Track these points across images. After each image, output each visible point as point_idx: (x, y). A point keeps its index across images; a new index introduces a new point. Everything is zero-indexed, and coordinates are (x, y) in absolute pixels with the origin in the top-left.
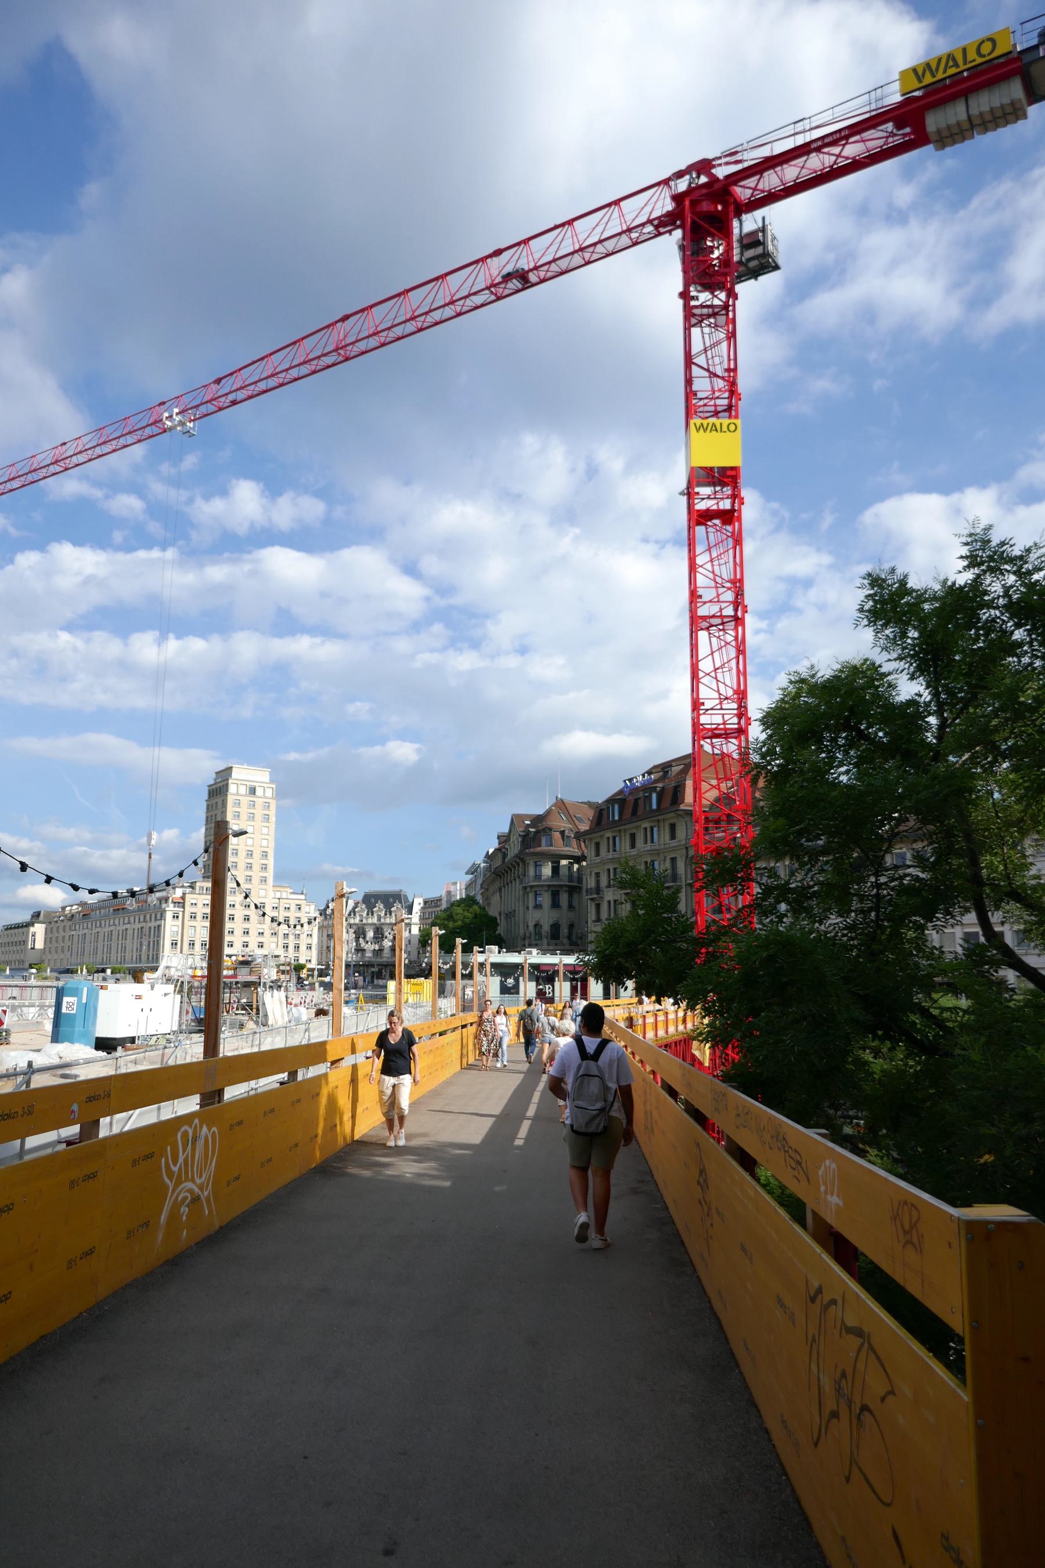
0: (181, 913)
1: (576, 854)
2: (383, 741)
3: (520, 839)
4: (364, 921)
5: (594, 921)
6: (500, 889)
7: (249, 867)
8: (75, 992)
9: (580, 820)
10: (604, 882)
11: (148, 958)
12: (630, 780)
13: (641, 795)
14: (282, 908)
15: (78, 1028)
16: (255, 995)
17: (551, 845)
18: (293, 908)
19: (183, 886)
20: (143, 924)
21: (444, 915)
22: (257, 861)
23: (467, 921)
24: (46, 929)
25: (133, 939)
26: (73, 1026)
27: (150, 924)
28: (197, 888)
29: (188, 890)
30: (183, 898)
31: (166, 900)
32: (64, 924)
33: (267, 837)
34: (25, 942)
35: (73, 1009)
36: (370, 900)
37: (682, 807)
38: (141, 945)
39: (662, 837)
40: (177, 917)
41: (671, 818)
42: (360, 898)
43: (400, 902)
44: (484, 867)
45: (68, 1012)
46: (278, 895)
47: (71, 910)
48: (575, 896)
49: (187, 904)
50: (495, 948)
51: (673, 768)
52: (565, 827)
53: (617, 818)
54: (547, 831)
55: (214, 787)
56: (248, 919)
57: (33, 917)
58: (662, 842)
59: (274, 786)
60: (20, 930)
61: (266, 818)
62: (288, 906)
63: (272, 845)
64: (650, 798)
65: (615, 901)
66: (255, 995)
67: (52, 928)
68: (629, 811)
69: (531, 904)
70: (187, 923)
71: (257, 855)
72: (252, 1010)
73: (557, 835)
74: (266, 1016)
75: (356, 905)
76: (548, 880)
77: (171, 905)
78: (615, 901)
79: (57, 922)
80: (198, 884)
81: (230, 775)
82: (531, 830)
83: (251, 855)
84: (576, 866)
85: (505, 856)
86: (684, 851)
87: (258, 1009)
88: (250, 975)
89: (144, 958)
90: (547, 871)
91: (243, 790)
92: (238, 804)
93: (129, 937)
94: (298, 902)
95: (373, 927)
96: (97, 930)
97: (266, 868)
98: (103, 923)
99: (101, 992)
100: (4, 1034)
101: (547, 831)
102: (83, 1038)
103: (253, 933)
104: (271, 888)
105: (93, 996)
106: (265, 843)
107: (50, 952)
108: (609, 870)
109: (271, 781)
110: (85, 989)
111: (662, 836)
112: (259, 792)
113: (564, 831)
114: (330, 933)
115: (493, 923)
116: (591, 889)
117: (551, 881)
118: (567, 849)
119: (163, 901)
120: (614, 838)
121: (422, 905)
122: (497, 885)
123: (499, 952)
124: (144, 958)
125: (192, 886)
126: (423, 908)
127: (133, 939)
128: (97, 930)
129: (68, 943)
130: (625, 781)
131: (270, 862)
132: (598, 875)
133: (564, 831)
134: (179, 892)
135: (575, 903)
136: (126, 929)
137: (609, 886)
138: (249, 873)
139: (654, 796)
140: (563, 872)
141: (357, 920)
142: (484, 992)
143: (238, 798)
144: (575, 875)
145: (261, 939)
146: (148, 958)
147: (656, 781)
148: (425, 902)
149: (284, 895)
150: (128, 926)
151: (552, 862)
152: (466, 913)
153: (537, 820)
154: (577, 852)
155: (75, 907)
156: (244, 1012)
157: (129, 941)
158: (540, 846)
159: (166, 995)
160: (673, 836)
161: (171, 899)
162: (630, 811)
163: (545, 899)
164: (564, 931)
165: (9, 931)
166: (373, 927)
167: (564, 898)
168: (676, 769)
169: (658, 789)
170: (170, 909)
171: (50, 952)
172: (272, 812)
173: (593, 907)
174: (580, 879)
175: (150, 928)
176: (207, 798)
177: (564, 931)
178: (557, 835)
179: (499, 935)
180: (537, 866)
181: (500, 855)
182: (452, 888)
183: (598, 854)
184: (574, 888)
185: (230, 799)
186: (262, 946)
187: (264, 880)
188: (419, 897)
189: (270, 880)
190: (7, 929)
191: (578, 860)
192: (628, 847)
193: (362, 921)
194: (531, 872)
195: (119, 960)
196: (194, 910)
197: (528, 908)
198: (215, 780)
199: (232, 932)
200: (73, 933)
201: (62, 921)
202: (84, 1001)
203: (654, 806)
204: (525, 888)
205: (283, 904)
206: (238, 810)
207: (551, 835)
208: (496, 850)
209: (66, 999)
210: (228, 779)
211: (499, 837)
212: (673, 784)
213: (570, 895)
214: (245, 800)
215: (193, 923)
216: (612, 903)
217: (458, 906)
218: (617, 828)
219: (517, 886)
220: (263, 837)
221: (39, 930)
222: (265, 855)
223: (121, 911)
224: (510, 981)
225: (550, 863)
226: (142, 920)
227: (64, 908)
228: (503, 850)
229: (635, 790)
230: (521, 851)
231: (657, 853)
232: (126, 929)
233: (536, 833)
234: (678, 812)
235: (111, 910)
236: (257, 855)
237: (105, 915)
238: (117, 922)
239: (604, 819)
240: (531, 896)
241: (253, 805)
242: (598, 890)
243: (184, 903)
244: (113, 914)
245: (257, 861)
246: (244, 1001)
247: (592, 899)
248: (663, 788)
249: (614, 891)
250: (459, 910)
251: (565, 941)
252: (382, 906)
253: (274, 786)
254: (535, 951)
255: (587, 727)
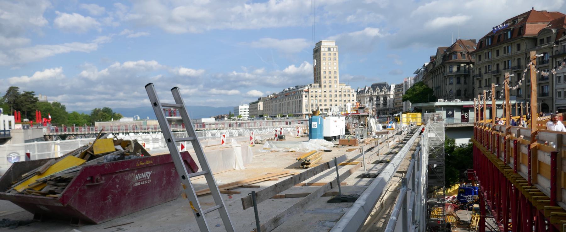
0: (308, 95)
1: (468, 62)
2: (363, 29)
3: (442, 57)
4: (372, 94)
5: (478, 88)
6: (432, 79)
7: (330, 77)
8: (316, 120)
9: (468, 47)
10: (483, 71)
11: (298, 111)
12: (496, 27)
13: (502, 33)
14: (343, 91)
15: (318, 133)
16: (366, 120)
17: (457, 58)
18: (347, 91)
19: (308, 86)
20: (285, 102)
21: (411, 89)
22: (333, 75)
23: (421, 91)
24: (263, 103)
25: (292, 105)
26: (317, 133)
27: (298, 100)
28: (313, 86)
29: (310, 87)
30: (308, 90)
31: (303, 91)
32: (269, 101)
33: (336, 66)
34: (257, 108)
35: (316, 126)
36: (374, 87)
37: (524, 36)
38: (295, 107)
39: (493, 55)
40: (307, 97)
41: (518, 41)
42: (370, 86)
43: (386, 87)
44: (423, 70)
45: (314, 127)
46: (341, 87)
47: (271, 96)
48: (467, 79)
49: (310, 92)
50: (442, 100)
51: (518, 20)
52: (462, 51)
53: (490, 44)
54: (455, 53)
55: (316, 49)
56: (331, 96)
57: (258, 99)
58: (493, 57)
59: (337, 47)
60: (255, 104)
61: (335, 59)
62: (345, 90)
63: (338, 69)
64: (507, 34)
65: (489, 79)
66: (366, 120)
67: (265, 103)
68: (496, 40)
69: (448, 83)
70: (311, 98)
71: (333, 72)
72: (365, 126)
73: (459, 54)
74: (371, 127)
75: (369, 89)
76: (455, 72)
77: (304, 93)
78: (489, 79)
79: (266, 101)
80: (313, 85)
81: (321, 44)
82: (447, 53)
83: (331, 73)
84: (467, 66)
85: (434, 65)
86: (525, 55)
87: (368, 125)
88: (364, 112)
89: (297, 111)
90: (455, 69)
91: (326, 49)
92: (325, 54)
93: (291, 104)
94: (348, 89)
95: (376, 96)
96: (289, 101)
97: (336, 77)
98: (282, 100)
99: (324, 120)
100: (284, 137)
101: (455, 53)
102: (320, 137)
103: (333, 101)
104: (338, 85)
105: (322, 122)
106: (335, 68)
107: (265, 111)
108: (486, 66)
109: (336, 45)
110: (320, 119)
111: (513, 49)
112: (332, 50)
113: (462, 52)
114: (360, 99)
115: (431, 91)
116: (477, 75)
117: (457, 73)
118: (464, 59)
119: (301, 92)
120: (489, 53)
121: (394, 87)
122: (431, 77)
123: (444, 101)
124: (297, 111)
125: (311, 85)
126: (395, 88)
127: (292, 105)
128: (289, 101)
129: (271, 108)
130: (494, 28)
131: (338, 75)
132: (480, 69)
133: (462, 52)
134: (307, 88)
135: (467, 81)
136: (290, 102)
137: (486, 73)
138: (330, 80)
139: (509, 33)
140: (462, 69)
141: (370, 94)
142: (441, 117)
143: (324, 52)
144: (467, 70)
145: (336, 103)
146: (298, 111)
147: (510, 26)
148: (396, 86)
149: (343, 87)
150: (290, 101)
151: (457, 65)
152: (420, 88)
153: (449, 49)
154: (468, 61)
155: (272, 95)
156: (362, 127)
157: (291, 106)
158: (451, 59)
159: (343, 120)
160: (519, 49)
161: (304, 91)
162: (497, 40)
163: (454, 80)
164: (463, 93)
165: (251, 105)
166: (376, 96)
167: (462, 80)
168: (520, 20)
169: (511, 29)
170: (304, 94)
171: (265, 111)
172: (337, 57)
173: (478, 82)
174: (469, 72)
175: (298, 101)
176: (313, 54)
177: (463, 93)
178: (459, 54)
179: (434, 95)
180: (451, 67)
181: (432, 65)
182: (407, 80)
183: (480, 60)
184: (467, 75)
185: (322, 53)
186: (326, 105)
187: (336, 82)
188: (393, 84)
189: (338, 82)
190: (251, 104)
191: (468, 64)
192: (495, 56)
193: (371, 94)
194: (448, 70)
195: (288, 112)
196: (312, 94)
197: (446, 84)
198: (316, 47)
199: (326, 101)
200: (272, 104)
201: (268, 100)
202: (319, 123)
203: (509, 37)
204: (445, 77)
205: (343, 90)
206: (325, 57)
207: (456, 55)
208: (430, 63)
209: (313, 123)
210: (320, 46)
211: (431, 58)
212: (519, 26)
213: (465, 78)
214: (327, 53)
215: (312, 98)
216: (487, 80)
217: (417, 85)
218: (490, 49)
219: (441, 77)
220: (334, 66)
221: (261, 104)
222: (335, 72)
223: (287, 96)
224: (450, 112)
225: (456, 66)
226: (295, 98)
227: (268, 96)
228: (433, 63)
229: (499, 31)
230: (442, 62)
231: (491, 62)
232: (290, 102)
233: (449, 54)
234: (522, 39)
235: (284, 95)
236: (333, 72)
237: (282, 97)
238: (286, 99)
239: (483, 46)
240: (448, 80)
241: (330, 55)
242: (480, 75)
243: (309, 92)
244: (285, 97)
245: (333, 75)
246: (362, 122)
247: (495, 76)
248: (514, 29)
249: (488, 75)
250: (418, 87)
251: (463, 96)
252: (379, 89)
253: (337, 47)
254: (459, 100)
255: (442, 15)
